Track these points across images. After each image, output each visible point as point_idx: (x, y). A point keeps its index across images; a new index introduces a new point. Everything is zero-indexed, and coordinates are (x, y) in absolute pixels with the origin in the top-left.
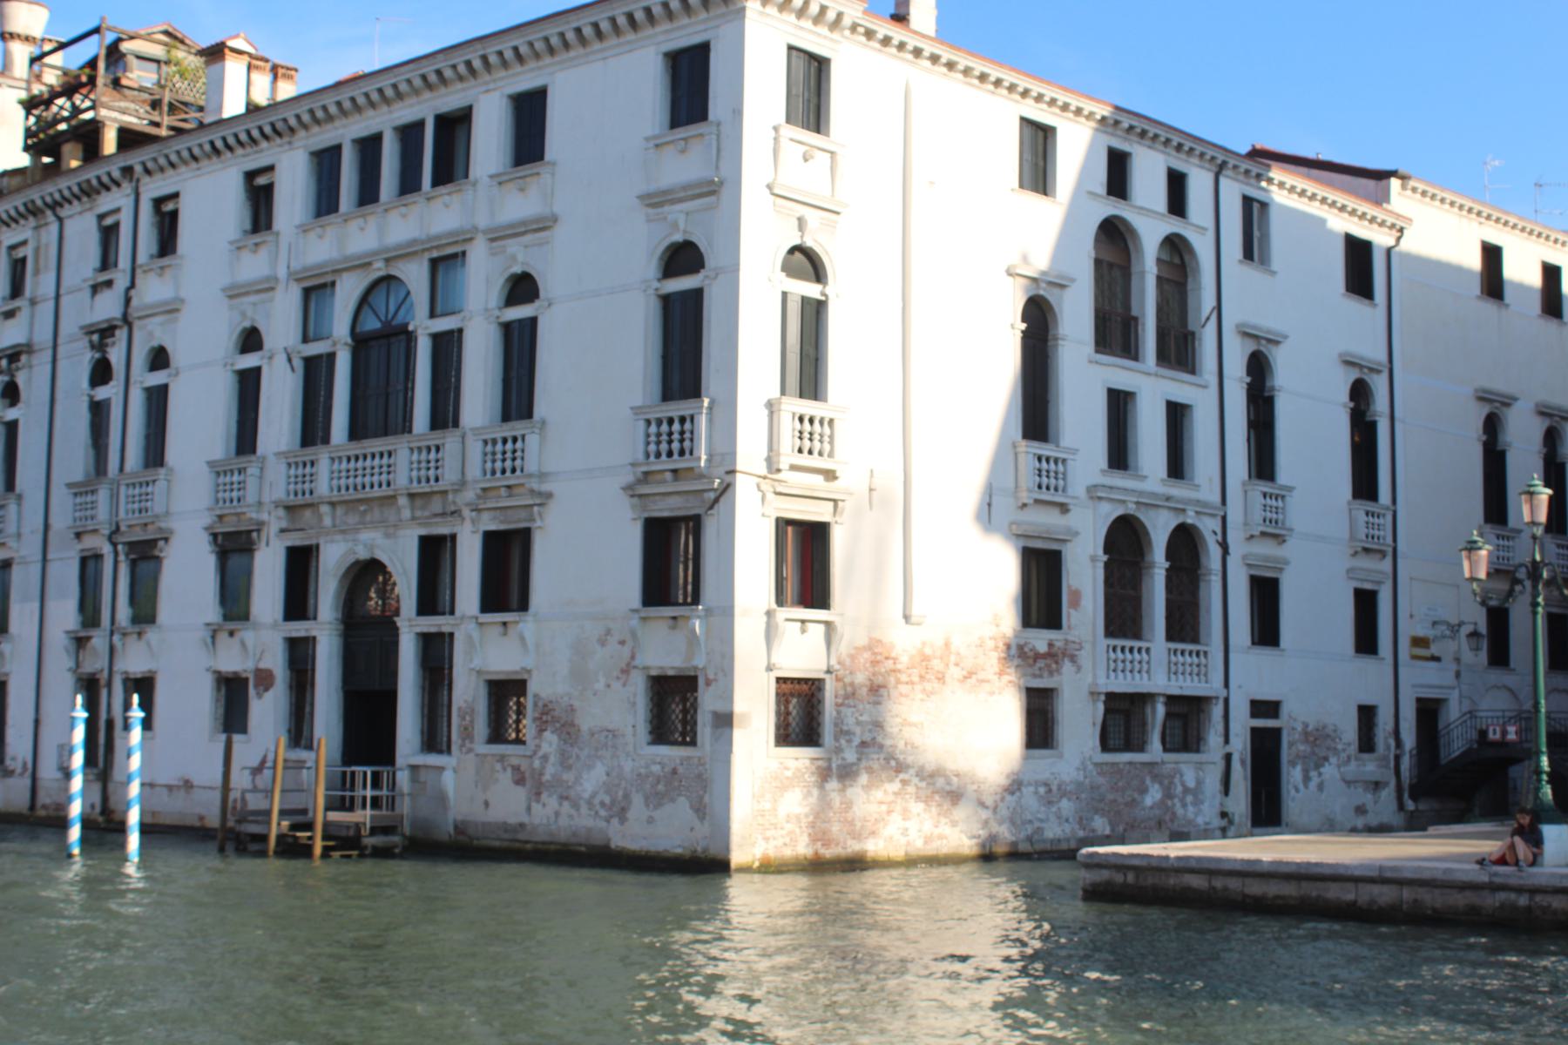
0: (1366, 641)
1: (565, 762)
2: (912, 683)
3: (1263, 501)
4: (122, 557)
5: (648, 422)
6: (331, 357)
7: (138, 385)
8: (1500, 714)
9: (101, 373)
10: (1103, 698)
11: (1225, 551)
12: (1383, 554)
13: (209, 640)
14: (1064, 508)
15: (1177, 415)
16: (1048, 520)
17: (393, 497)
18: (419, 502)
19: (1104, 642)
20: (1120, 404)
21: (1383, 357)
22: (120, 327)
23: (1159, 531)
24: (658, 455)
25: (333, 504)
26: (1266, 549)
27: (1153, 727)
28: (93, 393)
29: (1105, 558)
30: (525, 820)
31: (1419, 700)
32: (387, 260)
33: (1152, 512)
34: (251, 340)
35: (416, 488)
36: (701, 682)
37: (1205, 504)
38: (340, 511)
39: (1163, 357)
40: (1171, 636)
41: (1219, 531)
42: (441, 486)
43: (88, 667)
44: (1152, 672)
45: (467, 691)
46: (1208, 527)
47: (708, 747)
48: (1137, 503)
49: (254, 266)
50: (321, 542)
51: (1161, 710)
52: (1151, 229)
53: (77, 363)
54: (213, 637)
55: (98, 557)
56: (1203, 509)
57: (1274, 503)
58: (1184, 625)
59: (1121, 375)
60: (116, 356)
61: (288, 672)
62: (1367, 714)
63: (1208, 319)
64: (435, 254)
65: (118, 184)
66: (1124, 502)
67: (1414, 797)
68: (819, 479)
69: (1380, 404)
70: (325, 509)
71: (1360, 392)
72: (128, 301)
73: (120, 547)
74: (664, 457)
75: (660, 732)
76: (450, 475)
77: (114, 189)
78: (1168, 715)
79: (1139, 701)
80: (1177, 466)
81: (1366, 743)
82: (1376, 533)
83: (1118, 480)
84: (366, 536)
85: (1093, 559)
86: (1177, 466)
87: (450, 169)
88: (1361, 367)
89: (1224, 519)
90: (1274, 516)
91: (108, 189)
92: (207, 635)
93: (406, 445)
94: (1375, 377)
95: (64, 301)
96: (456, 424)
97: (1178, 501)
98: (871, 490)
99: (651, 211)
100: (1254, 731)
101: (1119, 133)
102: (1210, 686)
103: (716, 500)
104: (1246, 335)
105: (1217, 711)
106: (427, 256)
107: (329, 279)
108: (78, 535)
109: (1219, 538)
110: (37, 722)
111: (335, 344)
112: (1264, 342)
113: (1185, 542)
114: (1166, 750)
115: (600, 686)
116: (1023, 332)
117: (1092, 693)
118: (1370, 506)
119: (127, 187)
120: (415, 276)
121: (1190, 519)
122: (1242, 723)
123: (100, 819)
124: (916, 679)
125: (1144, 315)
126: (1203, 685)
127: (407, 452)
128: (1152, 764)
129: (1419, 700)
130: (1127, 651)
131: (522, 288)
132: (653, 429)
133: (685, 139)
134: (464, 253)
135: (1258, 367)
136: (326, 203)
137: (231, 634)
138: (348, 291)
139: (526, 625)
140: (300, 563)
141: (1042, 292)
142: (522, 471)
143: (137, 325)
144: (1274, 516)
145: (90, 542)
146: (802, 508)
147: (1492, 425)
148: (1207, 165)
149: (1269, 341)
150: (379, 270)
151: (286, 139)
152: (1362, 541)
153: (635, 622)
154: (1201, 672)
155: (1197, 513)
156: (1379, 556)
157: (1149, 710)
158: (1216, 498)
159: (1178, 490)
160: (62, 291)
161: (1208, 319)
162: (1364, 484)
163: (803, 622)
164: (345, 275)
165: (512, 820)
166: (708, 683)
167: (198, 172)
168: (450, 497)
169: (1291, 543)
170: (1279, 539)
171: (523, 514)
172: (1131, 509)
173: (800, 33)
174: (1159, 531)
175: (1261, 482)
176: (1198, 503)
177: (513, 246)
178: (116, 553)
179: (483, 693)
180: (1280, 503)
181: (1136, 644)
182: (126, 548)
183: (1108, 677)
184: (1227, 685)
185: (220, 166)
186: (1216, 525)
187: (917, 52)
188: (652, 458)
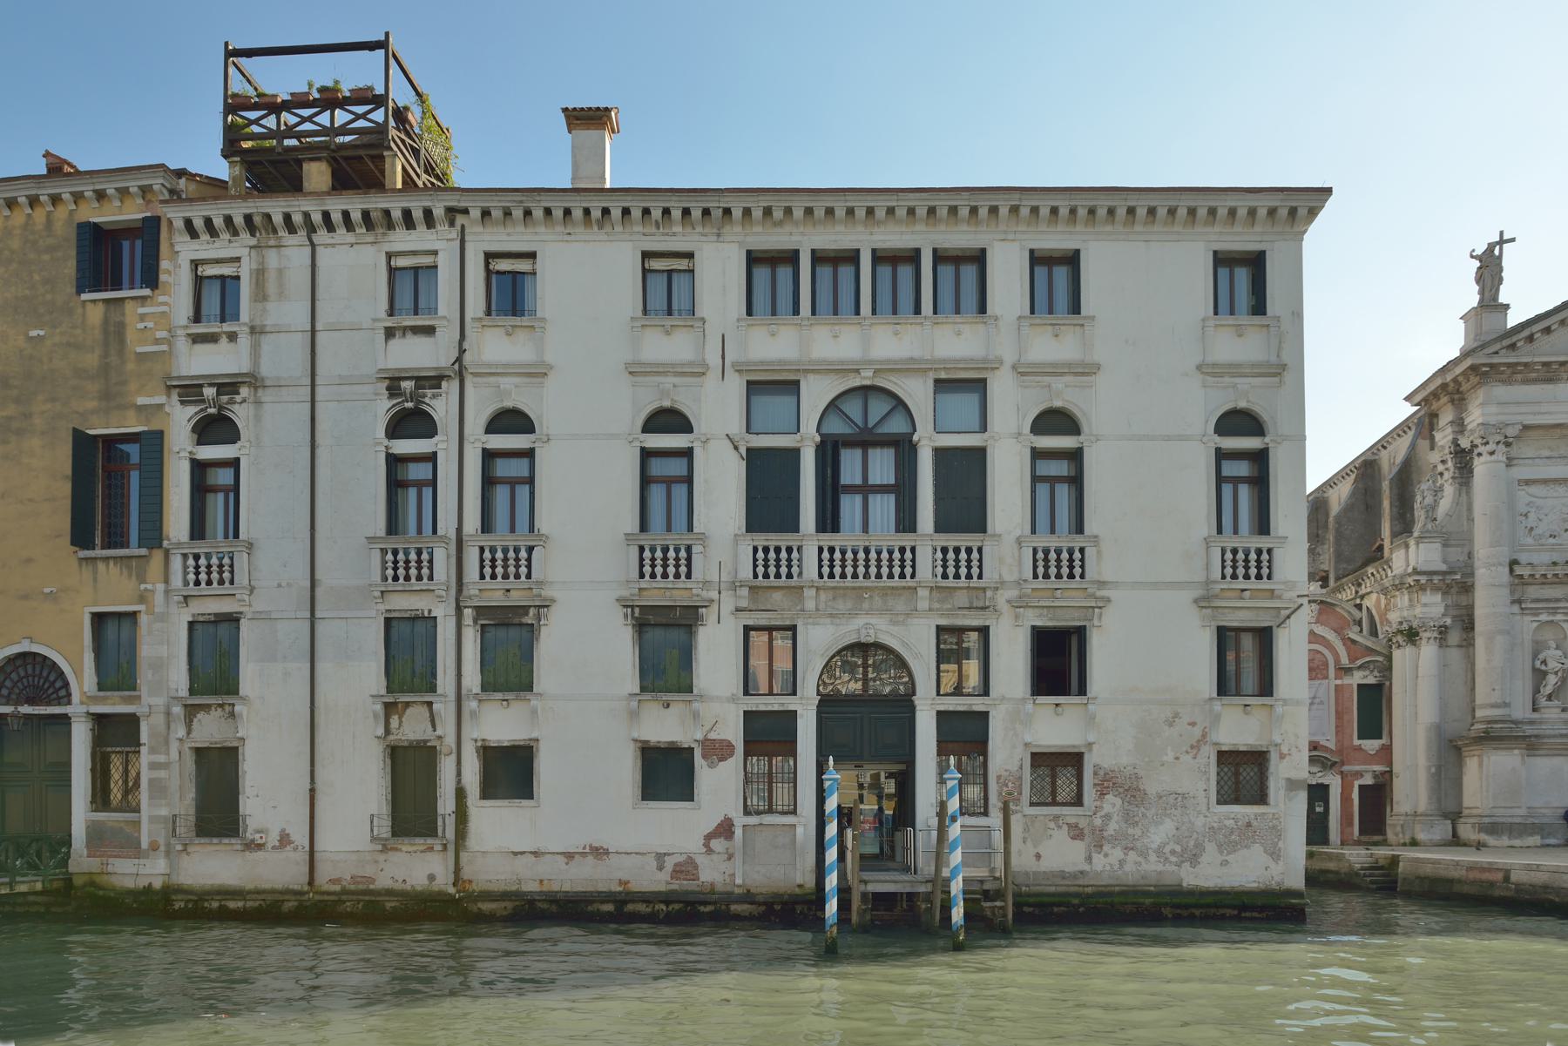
30: (1087, 868)
36: (1274, 757)
60: (441, 407)
84: (859, 622)
110: (312, 791)
150: (866, 378)
160: (319, 326)
164: (811, 377)
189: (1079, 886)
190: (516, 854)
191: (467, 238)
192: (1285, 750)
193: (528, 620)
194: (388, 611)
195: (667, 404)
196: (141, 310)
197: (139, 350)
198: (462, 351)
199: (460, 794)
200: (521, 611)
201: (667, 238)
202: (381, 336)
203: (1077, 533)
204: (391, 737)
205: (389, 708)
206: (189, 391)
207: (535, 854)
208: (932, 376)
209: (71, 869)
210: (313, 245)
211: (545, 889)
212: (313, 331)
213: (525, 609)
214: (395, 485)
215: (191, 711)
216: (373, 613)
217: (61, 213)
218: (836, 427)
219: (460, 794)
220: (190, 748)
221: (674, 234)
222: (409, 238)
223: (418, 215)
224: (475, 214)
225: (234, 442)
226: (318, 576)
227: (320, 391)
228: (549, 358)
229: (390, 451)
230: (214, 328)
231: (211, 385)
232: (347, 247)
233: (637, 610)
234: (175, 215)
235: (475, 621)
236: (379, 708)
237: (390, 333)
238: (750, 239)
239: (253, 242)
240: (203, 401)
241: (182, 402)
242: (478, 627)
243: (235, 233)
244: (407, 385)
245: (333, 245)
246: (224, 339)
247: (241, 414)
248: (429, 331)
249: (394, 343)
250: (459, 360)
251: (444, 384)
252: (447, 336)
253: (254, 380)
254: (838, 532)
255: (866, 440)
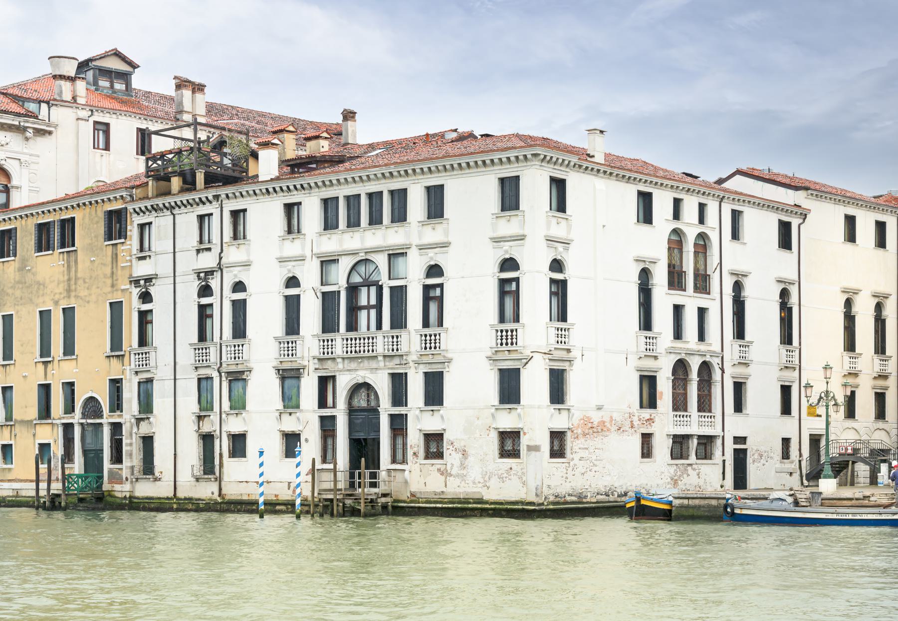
0: (786, 409)
1: (463, 466)
2: (598, 432)
3: (739, 349)
4: (224, 378)
5: (497, 331)
6: (339, 292)
7: (228, 299)
8: (845, 441)
9: (205, 291)
10: (672, 437)
11: (723, 372)
12: (794, 369)
13: (279, 417)
14: (656, 358)
15: (702, 312)
16: (649, 364)
17: (376, 357)
18: (387, 359)
19: (672, 413)
20: (678, 310)
21: (797, 279)
22: (217, 271)
23: (695, 364)
24: (502, 344)
25: (343, 359)
26: (741, 370)
27: (692, 449)
28: (199, 300)
29: (673, 378)
30: (444, 489)
31: (810, 435)
32: (366, 253)
33: (692, 357)
34: (293, 282)
35: (387, 353)
36: (522, 434)
37: (714, 352)
38: (346, 361)
39: (697, 289)
40: (700, 409)
41: (720, 363)
42: (400, 352)
43: (206, 428)
44: (692, 425)
45: (414, 439)
46: (715, 362)
47: (525, 458)
48: (686, 354)
49: (293, 248)
50: (337, 374)
51: (695, 441)
52: (691, 234)
53: (189, 288)
54: (280, 416)
55: (209, 379)
56: (713, 354)
57: (744, 349)
58: (704, 405)
59: (678, 298)
60: (214, 283)
61: (320, 431)
62: (786, 442)
63: (716, 269)
64: (391, 252)
65: (210, 202)
66: (680, 353)
67: (808, 480)
68: (565, 353)
69: (793, 300)
70: (339, 360)
71: (784, 294)
72: (221, 258)
73: (223, 374)
74: (504, 345)
75: (505, 453)
76: (404, 348)
77: (208, 204)
78: (698, 444)
79: (685, 438)
80: (702, 337)
81: (786, 455)
82: (791, 359)
83: (678, 344)
84: (361, 373)
85: (668, 378)
86: (702, 337)
87: (400, 216)
88: (785, 282)
89: (722, 358)
90: (744, 355)
91: (204, 203)
92: (278, 414)
93: (382, 335)
94: (791, 286)
95: (177, 254)
96: (406, 327)
97: (703, 352)
98: (583, 355)
99: (494, 244)
100: (735, 450)
101: (678, 191)
102: (715, 431)
103: (527, 363)
104: (732, 274)
105: (719, 442)
106: (387, 253)
107: (336, 258)
108: (196, 368)
109: (720, 366)
110: (175, 454)
111: (339, 287)
112: (740, 276)
113: (706, 367)
114: (697, 459)
115: (478, 435)
116: (639, 284)
117: (667, 435)
118: (789, 347)
119: (216, 204)
120: (381, 261)
121: (708, 359)
122: (730, 446)
123: (219, 500)
124: (600, 431)
125: (688, 271)
126: (713, 430)
127: (382, 337)
128: (690, 465)
129: (810, 435)
130: (678, 416)
131: (435, 270)
132: (499, 333)
133: (509, 216)
134: (406, 253)
135: (738, 287)
136: (330, 224)
137: (290, 414)
138: (345, 264)
139: (443, 411)
140: (325, 383)
141: (647, 266)
142: (439, 348)
143: (225, 270)
144: (744, 355)
145: (203, 372)
146: (559, 364)
147: (848, 303)
148: (716, 199)
149: (743, 275)
150: (362, 256)
151: (307, 191)
152: (784, 364)
153: (493, 410)
154: (712, 425)
155: (711, 356)
156: (792, 370)
157: (690, 442)
158: (718, 349)
159: (702, 347)
160: (176, 250)
161: (716, 269)
162: (787, 338)
163: (559, 409)
164: (343, 257)
165: (438, 490)
166: (525, 434)
167: (257, 201)
168: (404, 357)
169: (752, 366)
170: (746, 365)
171: (440, 366)
172: (683, 356)
173: (555, 171)
174: (695, 364)
175: (739, 340)
176: (709, 351)
177: (431, 253)
178: (221, 376)
179: (422, 438)
180: (747, 349)
181: (685, 414)
182: (226, 374)
183: (674, 428)
184: (723, 430)
185: (270, 199)
186: (719, 360)
187: (598, 171)
188: (499, 346)
189: (442, 499)
190: (240, 482)
191: (223, 206)
192: (526, 431)
193: (244, 377)
194: (199, 375)
195: (507, 256)
196: (122, 248)
197: (122, 265)
198: (221, 258)
199: (221, 455)
200: (242, 373)
201: (292, 197)
202: (195, 253)
203: (514, 322)
204: (200, 431)
205: (200, 418)
206: (136, 282)
207: (246, 482)
208: (387, 253)
209: (104, 489)
210: (174, 215)
211: (250, 498)
212: (174, 252)
213: (243, 372)
214: (503, 294)
215: (139, 420)
216: (193, 376)
217: (99, 209)
218: (356, 279)
219: (221, 455)
220: (139, 437)
221: (294, 195)
222: (203, 208)
223: (271, 190)
224: (224, 196)
225: (441, 277)
226: (177, 361)
227: (177, 279)
228: (251, 259)
229: (201, 303)
230: (147, 254)
231: (143, 279)
232: (185, 214)
233: (281, 371)
234: (130, 208)
235: (227, 378)
236: (194, 418)
237: (198, 251)
238: (321, 194)
239: (156, 215)
240: (140, 286)
241: (135, 287)
242: (228, 381)
243: (151, 212)
244: (142, 282)
245: (181, 214)
246: (148, 258)
247: (152, 290)
248: (209, 249)
249: (200, 255)
250: (219, 263)
251: (215, 273)
252: (216, 250)
253: (156, 276)
254: (146, 346)
255: (368, 284)
